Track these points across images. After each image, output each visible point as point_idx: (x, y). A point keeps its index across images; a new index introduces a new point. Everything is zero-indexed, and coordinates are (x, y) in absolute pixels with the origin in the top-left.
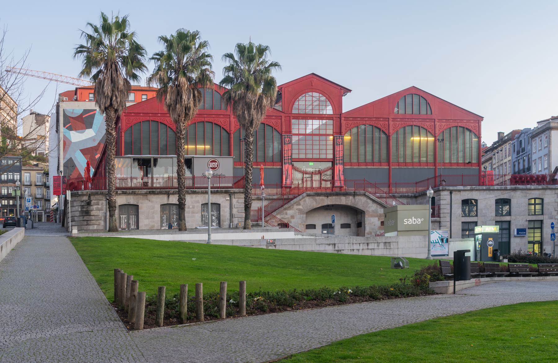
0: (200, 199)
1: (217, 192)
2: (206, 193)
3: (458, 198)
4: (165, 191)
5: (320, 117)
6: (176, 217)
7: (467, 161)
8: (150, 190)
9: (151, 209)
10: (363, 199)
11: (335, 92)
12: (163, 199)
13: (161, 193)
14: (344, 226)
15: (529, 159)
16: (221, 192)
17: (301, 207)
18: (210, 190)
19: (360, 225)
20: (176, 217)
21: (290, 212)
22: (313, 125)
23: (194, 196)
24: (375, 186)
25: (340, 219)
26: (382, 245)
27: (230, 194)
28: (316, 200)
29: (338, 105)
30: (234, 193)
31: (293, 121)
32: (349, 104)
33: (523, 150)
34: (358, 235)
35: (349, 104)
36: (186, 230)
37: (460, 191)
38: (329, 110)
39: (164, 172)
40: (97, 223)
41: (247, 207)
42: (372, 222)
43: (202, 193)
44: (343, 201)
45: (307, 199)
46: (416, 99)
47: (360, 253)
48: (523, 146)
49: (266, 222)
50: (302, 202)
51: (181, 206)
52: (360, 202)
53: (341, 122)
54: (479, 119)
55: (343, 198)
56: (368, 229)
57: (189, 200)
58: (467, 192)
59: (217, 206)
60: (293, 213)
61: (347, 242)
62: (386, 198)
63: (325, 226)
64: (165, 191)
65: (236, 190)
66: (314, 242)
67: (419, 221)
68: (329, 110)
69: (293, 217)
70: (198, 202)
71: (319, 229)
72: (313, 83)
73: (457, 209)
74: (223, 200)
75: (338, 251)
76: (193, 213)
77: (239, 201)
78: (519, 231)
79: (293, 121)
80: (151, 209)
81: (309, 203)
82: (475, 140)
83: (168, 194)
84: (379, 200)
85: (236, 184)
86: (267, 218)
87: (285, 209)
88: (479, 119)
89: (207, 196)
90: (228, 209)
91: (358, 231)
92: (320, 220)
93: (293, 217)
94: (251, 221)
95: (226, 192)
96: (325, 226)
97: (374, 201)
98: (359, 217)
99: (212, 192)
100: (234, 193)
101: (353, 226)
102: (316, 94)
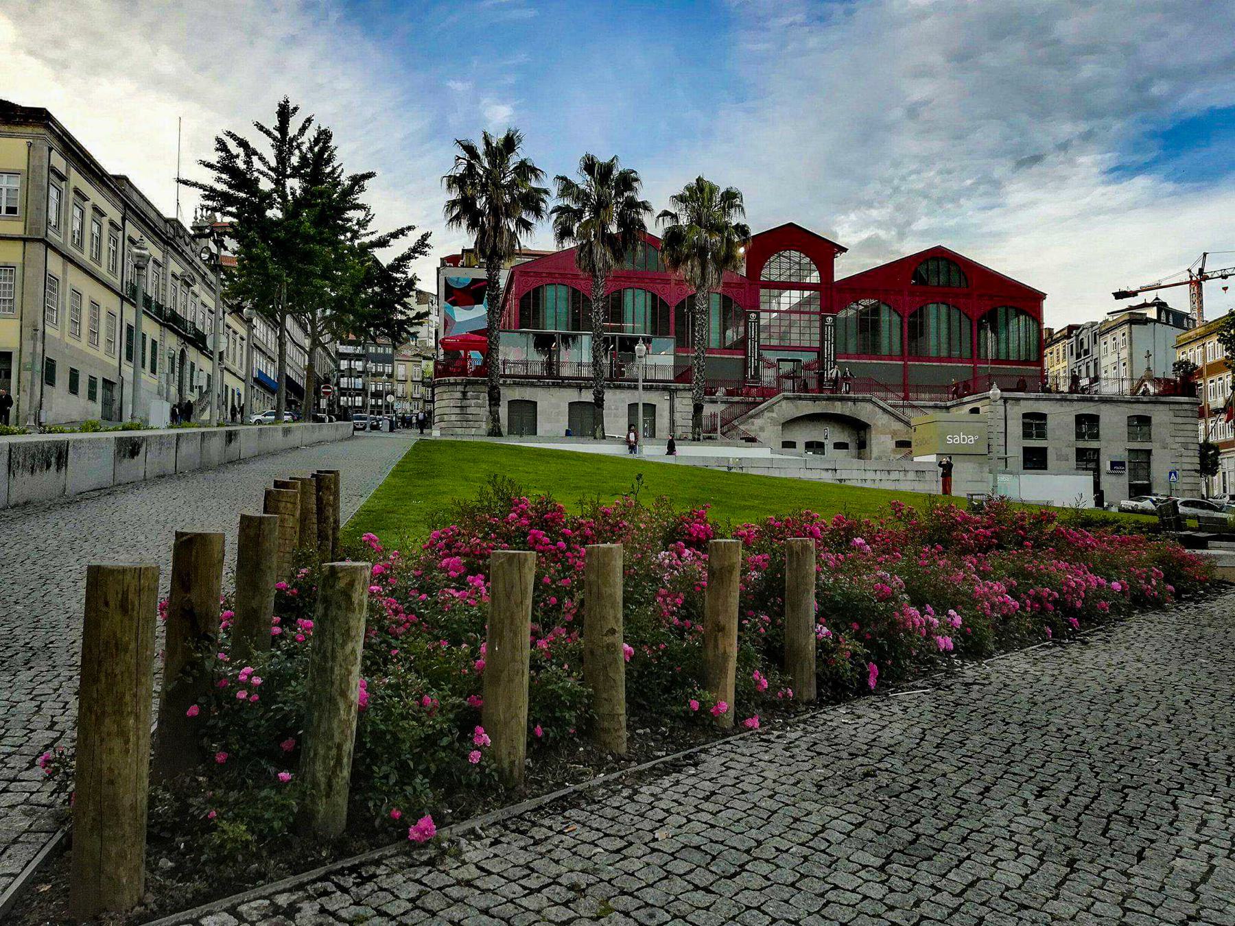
0: (627, 397)
1: (651, 388)
2: (636, 388)
3: (1016, 412)
4: (578, 383)
5: (801, 287)
6: (586, 420)
7: (1023, 358)
8: (552, 377)
9: (553, 407)
10: (869, 406)
11: (823, 251)
12: (572, 395)
13: (569, 386)
14: (838, 446)
15: (1096, 365)
16: (657, 389)
17: (774, 415)
18: (641, 384)
19: (862, 445)
20: (586, 420)
21: (758, 422)
22: (791, 298)
23: (618, 392)
24: (886, 388)
25: (830, 435)
26: (911, 475)
27: (672, 392)
28: (797, 407)
29: (826, 269)
30: (677, 390)
31: (762, 291)
32: (843, 268)
33: (1086, 352)
34: (859, 458)
35: (843, 268)
36: (604, 437)
37: (1018, 400)
38: (815, 278)
39: (578, 356)
40: (477, 425)
41: (698, 409)
42: (882, 442)
43: (629, 387)
44: (838, 408)
45: (784, 403)
46: (942, 264)
47: (877, 485)
48: (1086, 347)
49: (723, 434)
50: (776, 408)
51: (599, 402)
52: (864, 412)
53: (833, 295)
54: (1038, 297)
55: (838, 404)
56: (875, 453)
57: (609, 396)
58: (1031, 402)
59: (650, 409)
60: (766, 423)
61: (855, 467)
62: (903, 406)
63: (810, 446)
64: (578, 383)
65: (681, 386)
66: (797, 467)
67: (971, 440)
68: (815, 278)
69: (762, 429)
70: (623, 401)
71: (801, 447)
72: (790, 237)
73: (1016, 428)
74: (661, 401)
75: (840, 480)
76: (615, 416)
77: (684, 404)
78: (1113, 464)
79: (762, 291)
80: (553, 407)
81: (788, 409)
82: (1033, 326)
83: (580, 388)
84: (890, 409)
85: (678, 379)
86: (725, 429)
87: (752, 417)
88: (1038, 297)
89: (636, 393)
90: (667, 414)
91: (859, 453)
92: (802, 436)
93: (762, 429)
94: (702, 431)
95: (665, 389)
96: (810, 446)
97: (884, 410)
98: (862, 433)
99: (644, 388)
100: (677, 390)
101: (852, 446)
102: (795, 255)
